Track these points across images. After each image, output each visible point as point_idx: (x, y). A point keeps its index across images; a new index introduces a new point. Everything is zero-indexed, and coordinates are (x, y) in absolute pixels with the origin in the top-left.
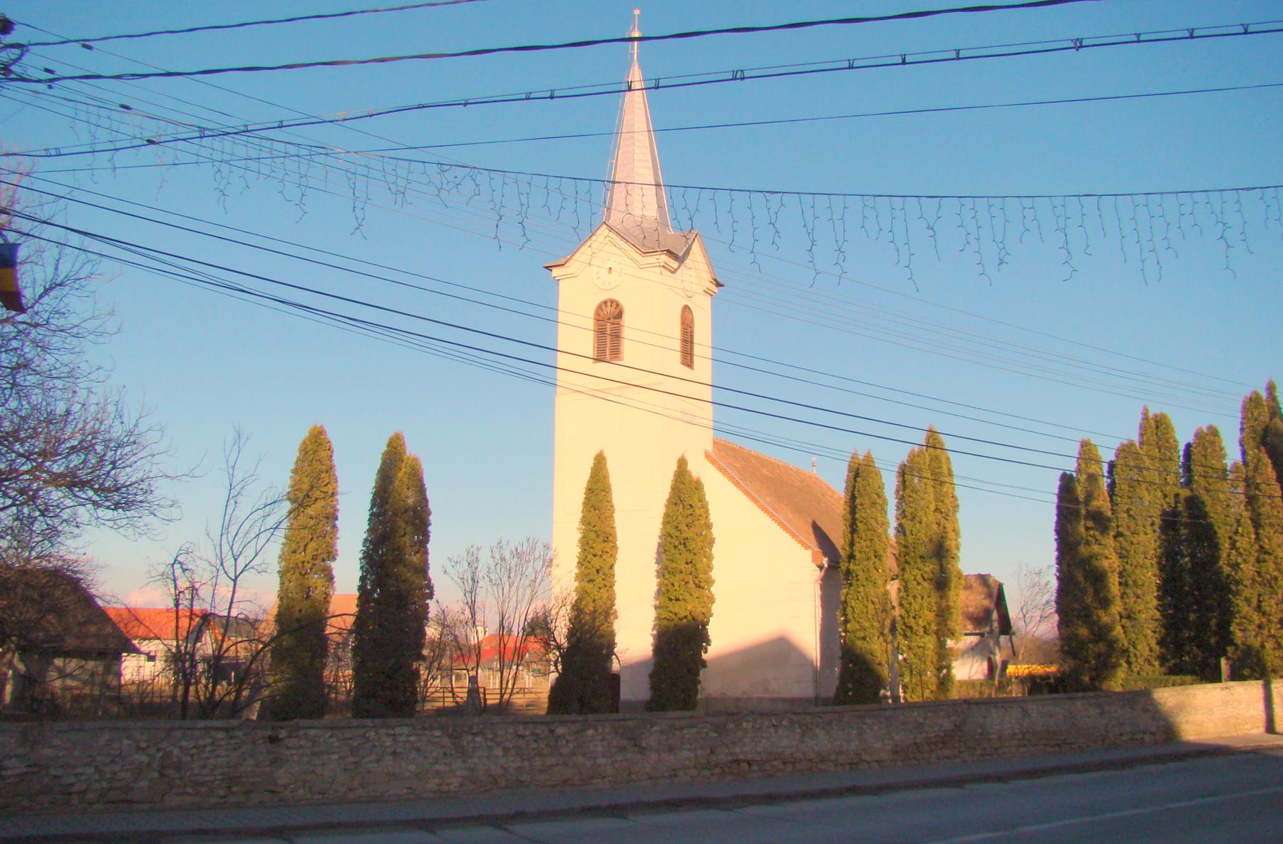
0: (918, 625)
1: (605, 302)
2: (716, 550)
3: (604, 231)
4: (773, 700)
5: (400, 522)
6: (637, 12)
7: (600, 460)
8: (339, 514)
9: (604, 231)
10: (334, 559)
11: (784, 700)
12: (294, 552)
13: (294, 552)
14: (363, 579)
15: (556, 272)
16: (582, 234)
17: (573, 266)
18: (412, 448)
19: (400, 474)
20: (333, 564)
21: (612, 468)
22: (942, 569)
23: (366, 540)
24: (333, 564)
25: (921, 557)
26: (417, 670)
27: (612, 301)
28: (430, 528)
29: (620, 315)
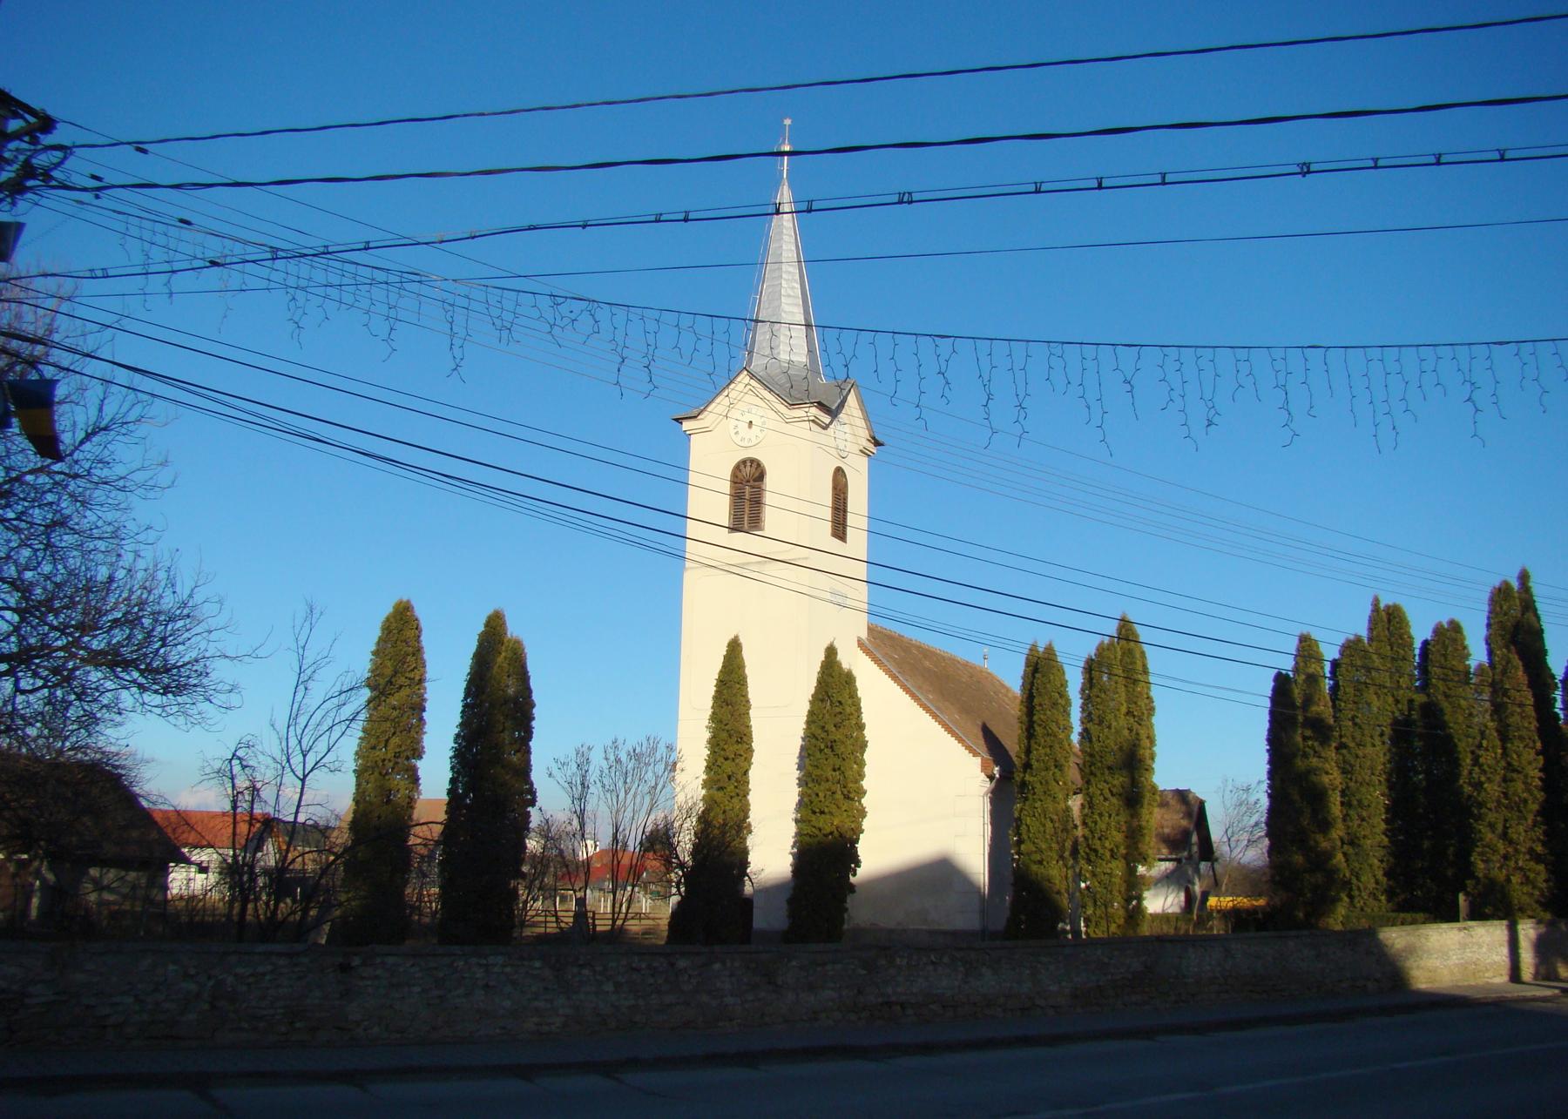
0: (1104, 847)
1: (744, 462)
2: (868, 756)
3: (744, 378)
4: (931, 933)
5: (500, 707)
6: (788, 122)
7: (734, 647)
8: (427, 705)
9: (744, 378)
10: (420, 757)
11: (945, 933)
12: (374, 748)
13: (374, 748)
14: (453, 781)
15: (686, 425)
16: (719, 383)
17: (707, 419)
18: (514, 629)
19: (500, 659)
20: (419, 764)
21: (748, 655)
22: (1134, 782)
23: (458, 736)
24: (419, 764)
25: (1109, 768)
26: (516, 890)
27: (752, 461)
28: (534, 723)
29: (760, 476)
